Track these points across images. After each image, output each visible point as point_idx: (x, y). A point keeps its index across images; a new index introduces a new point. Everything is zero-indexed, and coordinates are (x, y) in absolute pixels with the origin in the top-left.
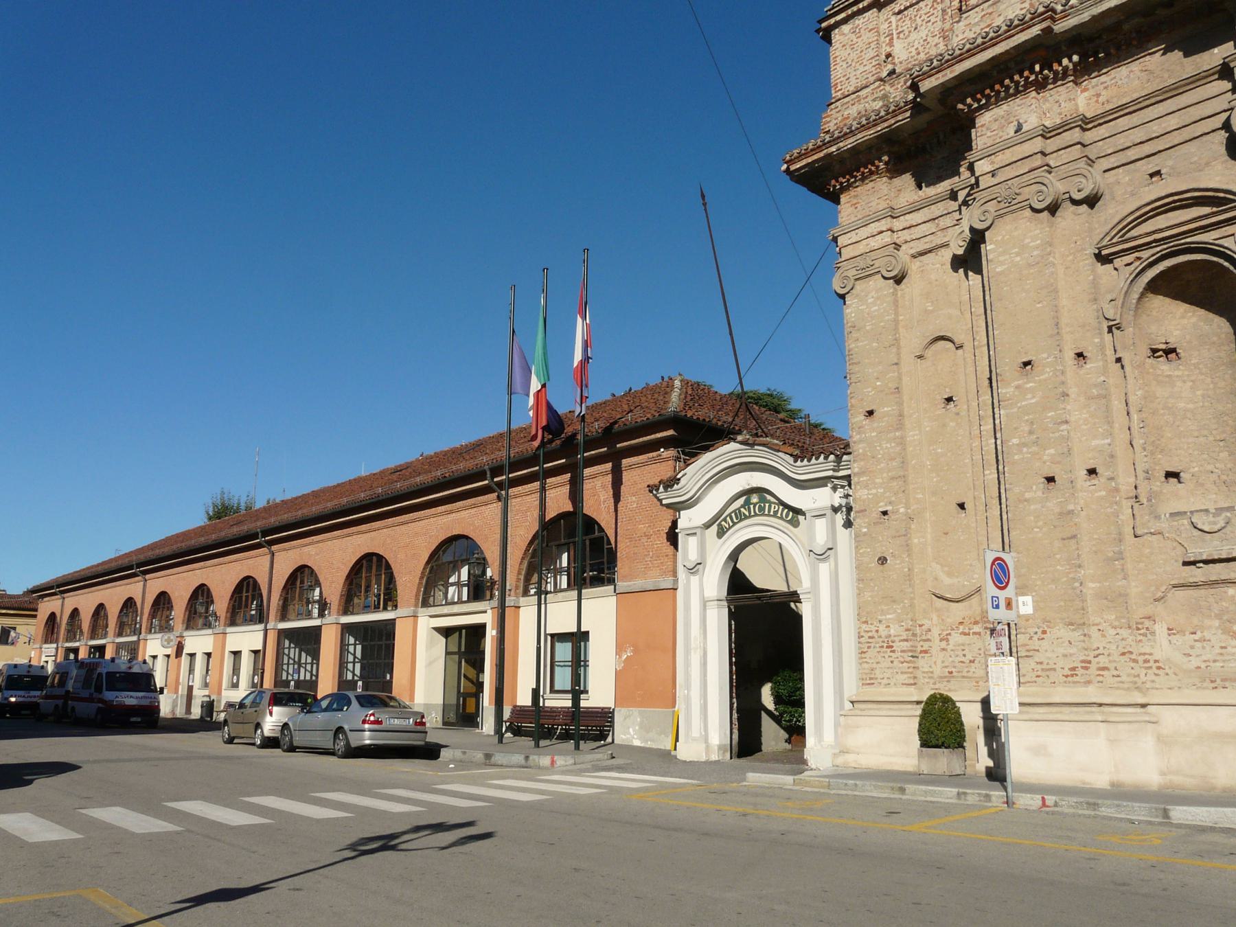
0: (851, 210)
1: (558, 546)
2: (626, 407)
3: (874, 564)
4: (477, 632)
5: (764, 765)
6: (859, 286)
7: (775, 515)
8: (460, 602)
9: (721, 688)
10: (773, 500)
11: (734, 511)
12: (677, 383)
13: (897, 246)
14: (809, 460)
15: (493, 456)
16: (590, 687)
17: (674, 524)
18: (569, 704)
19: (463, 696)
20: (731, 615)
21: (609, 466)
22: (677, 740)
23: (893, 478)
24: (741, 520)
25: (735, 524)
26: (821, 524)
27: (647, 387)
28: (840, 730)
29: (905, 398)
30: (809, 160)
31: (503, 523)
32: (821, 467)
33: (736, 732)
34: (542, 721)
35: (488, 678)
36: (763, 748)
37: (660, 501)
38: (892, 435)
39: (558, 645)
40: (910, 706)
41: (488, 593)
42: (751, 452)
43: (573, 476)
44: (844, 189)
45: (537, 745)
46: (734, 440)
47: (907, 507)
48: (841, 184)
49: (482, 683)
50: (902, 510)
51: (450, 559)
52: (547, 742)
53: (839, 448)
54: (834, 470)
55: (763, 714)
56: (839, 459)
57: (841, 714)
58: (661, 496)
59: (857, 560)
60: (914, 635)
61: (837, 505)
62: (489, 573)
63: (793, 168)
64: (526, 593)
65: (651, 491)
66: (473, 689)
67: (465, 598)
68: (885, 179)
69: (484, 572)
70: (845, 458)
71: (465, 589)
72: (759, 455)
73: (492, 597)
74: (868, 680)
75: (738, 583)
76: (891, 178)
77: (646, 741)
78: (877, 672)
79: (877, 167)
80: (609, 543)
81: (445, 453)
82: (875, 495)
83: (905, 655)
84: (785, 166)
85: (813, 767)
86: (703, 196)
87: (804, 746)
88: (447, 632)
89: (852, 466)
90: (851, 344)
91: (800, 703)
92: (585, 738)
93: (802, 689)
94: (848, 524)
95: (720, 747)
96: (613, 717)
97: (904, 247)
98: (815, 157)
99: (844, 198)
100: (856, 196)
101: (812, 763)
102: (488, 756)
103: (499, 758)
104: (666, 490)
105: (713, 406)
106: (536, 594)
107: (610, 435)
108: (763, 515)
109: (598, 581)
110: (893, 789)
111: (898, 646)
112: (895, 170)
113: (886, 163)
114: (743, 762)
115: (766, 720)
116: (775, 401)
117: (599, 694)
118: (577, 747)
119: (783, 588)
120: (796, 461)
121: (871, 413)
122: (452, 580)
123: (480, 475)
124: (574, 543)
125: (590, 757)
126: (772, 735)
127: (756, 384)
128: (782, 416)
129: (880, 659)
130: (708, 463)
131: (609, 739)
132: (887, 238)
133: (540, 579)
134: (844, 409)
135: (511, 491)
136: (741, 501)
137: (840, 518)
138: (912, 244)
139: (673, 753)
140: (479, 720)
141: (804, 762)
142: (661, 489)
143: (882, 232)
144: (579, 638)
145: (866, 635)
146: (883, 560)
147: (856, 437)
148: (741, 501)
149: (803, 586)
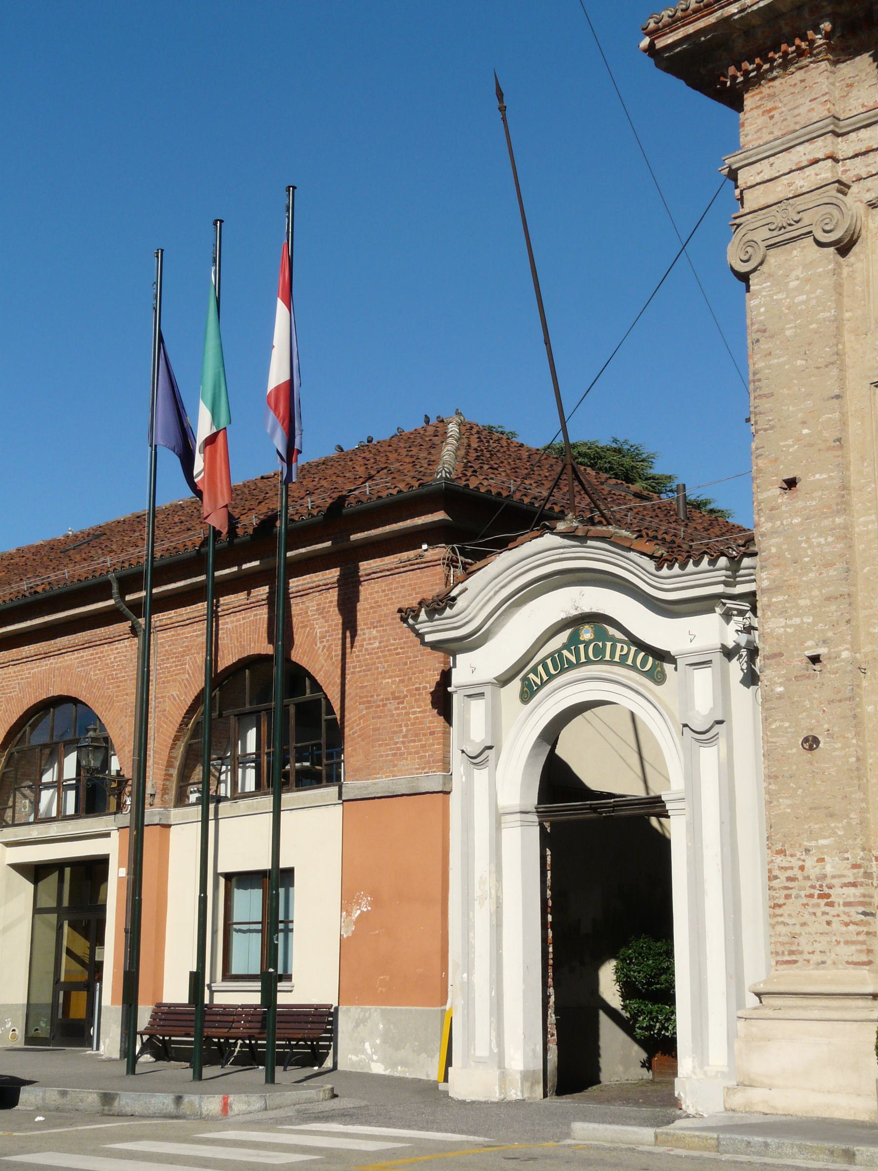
0: (761, 121)
1: (240, 716)
2: (361, 471)
3: (796, 749)
4: (93, 870)
5: (603, 1108)
6: (775, 258)
7: (622, 662)
8: (61, 817)
9: (527, 968)
10: (619, 635)
11: (551, 655)
12: (453, 429)
13: (843, 187)
14: (683, 566)
15: (123, 556)
16: (295, 969)
17: (446, 677)
18: (255, 999)
19: (65, 989)
20: (545, 839)
21: (333, 574)
22: (449, 1062)
23: (828, 599)
24: (563, 671)
25: (551, 677)
26: (703, 679)
27: (399, 435)
28: (737, 1045)
29: (853, 457)
30: (691, 29)
31: (138, 677)
32: (703, 578)
33: (553, 1047)
34: (207, 1032)
35: (111, 955)
36: (604, 1076)
37: (421, 636)
38: (826, 523)
39: (239, 895)
40: (861, 1003)
41: (113, 801)
42: (581, 551)
43: (272, 597)
44: (750, 83)
45: (198, 1076)
46: (552, 530)
47: (855, 648)
48: (746, 73)
49: (100, 965)
50: (845, 654)
51: (45, 739)
52: (216, 1070)
53: (738, 546)
54: (726, 584)
55: (603, 1018)
56: (735, 563)
57: (739, 1016)
58: (422, 628)
59: (766, 742)
60: (868, 875)
61: (731, 645)
62: (115, 764)
63: (660, 43)
64: (181, 800)
65: (404, 620)
66: (81, 975)
67: (70, 810)
68: (824, 65)
69: (106, 764)
70: (746, 562)
71: (71, 795)
72: (596, 556)
73: (120, 808)
74: (786, 955)
75: (557, 782)
76: (835, 63)
77: (394, 1065)
78: (803, 940)
79: (812, 42)
80: (330, 710)
81: (37, 550)
82: (798, 627)
83: (852, 910)
84: (645, 42)
85: (691, 1111)
86: (500, 95)
87: (675, 1074)
88: (35, 872)
89: (759, 575)
90: (757, 362)
91: (667, 997)
92: (284, 1060)
93: (669, 971)
94: (751, 679)
95: (526, 1076)
96: (334, 1023)
97: (855, 188)
98: (701, 24)
99: (750, 100)
100: (772, 96)
101: (689, 1104)
102: (107, 1098)
103: (126, 1101)
104: (431, 618)
105: (515, 470)
106: (199, 801)
107: (338, 518)
108: (602, 661)
109: (309, 779)
110: (832, 1152)
111: (839, 894)
112: (843, 49)
113: (828, 36)
114: (566, 1102)
115: (605, 1022)
116: (627, 461)
117: (311, 981)
118: (270, 1079)
119: (636, 790)
120: (659, 568)
121: (791, 483)
122: (47, 778)
123: (100, 590)
124: (268, 710)
125: (292, 1095)
126: (618, 1054)
127: (591, 430)
128: (637, 487)
129: (807, 917)
130: (506, 569)
131: (328, 1063)
132: (825, 172)
133: (207, 774)
134: (745, 476)
135: (155, 618)
136: (563, 637)
137: (736, 668)
138: (869, 183)
139: (442, 1086)
140: (93, 1031)
141: (675, 1103)
142: (423, 616)
143: (816, 161)
144: (275, 881)
145: (783, 875)
146: (811, 743)
147: (766, 526)
148: (563, 637)
149: (671, 788)
